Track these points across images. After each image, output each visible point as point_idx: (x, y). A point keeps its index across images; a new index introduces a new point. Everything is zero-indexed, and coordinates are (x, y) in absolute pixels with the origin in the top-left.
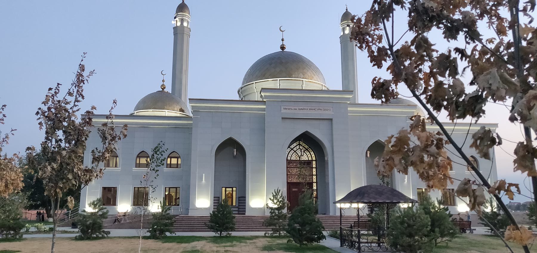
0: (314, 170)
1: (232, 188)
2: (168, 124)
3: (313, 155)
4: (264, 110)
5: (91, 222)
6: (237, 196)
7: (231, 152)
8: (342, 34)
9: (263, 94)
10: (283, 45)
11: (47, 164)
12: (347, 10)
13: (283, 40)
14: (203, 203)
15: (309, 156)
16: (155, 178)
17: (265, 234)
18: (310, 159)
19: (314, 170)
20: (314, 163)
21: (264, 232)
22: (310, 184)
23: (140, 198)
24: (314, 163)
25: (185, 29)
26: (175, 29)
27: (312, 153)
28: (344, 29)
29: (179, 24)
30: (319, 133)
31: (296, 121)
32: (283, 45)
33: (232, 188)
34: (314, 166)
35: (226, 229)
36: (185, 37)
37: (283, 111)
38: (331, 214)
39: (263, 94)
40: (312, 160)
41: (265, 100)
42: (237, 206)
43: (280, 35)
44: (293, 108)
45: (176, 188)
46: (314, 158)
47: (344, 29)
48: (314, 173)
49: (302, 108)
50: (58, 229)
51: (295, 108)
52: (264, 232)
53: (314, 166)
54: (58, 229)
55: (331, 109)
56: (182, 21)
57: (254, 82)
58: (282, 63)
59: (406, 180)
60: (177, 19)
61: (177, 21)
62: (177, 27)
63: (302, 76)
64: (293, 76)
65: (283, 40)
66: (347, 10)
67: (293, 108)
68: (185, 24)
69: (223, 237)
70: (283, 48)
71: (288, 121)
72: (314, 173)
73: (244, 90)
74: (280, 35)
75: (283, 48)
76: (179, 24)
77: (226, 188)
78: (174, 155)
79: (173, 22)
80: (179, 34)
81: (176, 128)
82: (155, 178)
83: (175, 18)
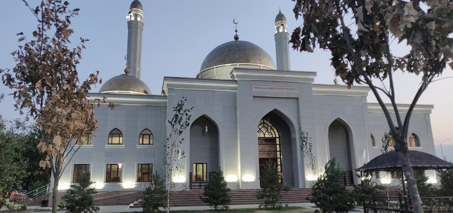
0: (278, 146)
1: (203, 164)
2: (141, 103)
3: (277, 133)
4: (235, 89)
5: (80, 197)
6: (208, 172)
7: (206, 128)
8: (277, 32)
9: (235, 74)
10: (236, 35)
11: (318, 5)
12: (280, 12)
13: (236, 31)
14: (179, 178)
15: (273, 133)
16: (180, 142)
17: (260, 206)
18: (274, 136)
19: (278, 146)
20: (278, 140)
21: (259, 205)
22: (275, 160)
23: (113, 177)
24: (278, 140)
25: (139, 24)
26: (130, 23)
27: (275, 130)
28: (278, 28)
29: (133, 19)
30: (287, 110)
31: (265, 100)
32: (236, 35)
33: (203, 164)
34: (278, 143)
35: (223, 203)
36: (139, 30)
37: (254, 90)
38: (301, 186)
39: (235, 74)
40: (276, 138)
41: (237, 79)
42: (208, 181)
43: (234, 27)
44: (263, 87)
45: (149, 164)
46: (277, 136)
47: (278, 28)
48: (278, 149)
49: (271, 87)
50: (28, 208)
51: (265, 87)
52: (259, 205)
53: (278, 143)
54: (28, 208)
55: (297, 88)
56: (136, 16)
57: (215, 67)
58: (235, 51)
59: (364, 154)
60: (131, 14)
61: (131, 16)
62: (131, 21)
63: (259, 62)
64: (251, 61)
65: (236, 31)
66: (280, 12)
67: (263, 87)
68: (139, 19)
69: (219, 210)
70: (236, 38)
71: (257, 99)
72: (278, 149)
73: (204, 75)
74: (234, 27)
75: (236, 38)
76: (133, 19)
77: (197, 164)
78: (146, 132)
79: (128, 17)
80: (133, 27)
81: (149, 106)
82: (180, 142)
83: (130, 13)
